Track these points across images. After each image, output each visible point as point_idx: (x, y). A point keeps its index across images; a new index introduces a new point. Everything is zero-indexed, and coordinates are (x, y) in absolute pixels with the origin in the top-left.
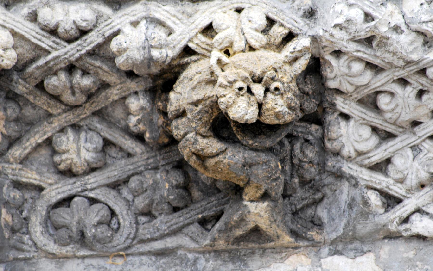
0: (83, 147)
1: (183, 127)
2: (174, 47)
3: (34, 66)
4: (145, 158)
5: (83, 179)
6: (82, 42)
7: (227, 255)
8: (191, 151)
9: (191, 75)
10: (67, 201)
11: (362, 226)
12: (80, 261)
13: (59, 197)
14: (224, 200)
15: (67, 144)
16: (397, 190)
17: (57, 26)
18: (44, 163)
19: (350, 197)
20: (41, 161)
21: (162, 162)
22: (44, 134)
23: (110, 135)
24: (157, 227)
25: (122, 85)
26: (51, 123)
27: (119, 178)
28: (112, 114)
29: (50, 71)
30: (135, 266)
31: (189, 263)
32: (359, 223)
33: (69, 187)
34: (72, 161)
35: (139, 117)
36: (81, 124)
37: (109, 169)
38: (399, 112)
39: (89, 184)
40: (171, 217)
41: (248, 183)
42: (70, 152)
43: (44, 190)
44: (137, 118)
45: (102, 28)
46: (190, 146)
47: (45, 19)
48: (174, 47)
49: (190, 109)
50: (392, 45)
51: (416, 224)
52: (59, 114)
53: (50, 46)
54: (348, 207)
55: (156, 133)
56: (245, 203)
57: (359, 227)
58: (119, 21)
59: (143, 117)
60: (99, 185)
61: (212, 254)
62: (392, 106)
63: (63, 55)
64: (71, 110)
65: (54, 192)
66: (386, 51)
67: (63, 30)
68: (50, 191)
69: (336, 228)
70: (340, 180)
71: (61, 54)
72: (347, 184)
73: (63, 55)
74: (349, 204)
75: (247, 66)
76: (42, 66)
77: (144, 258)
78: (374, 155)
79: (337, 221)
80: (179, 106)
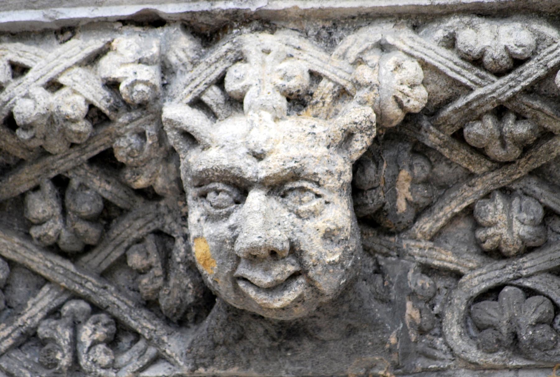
0: (516, 218)
3: (451, 108)
10: (493, 293)
17: (483, 53)
18: (463, 240)
20: (458, 237)
22: (464, 201)
26: (473, 185)
29: (472, 115)
33: (497, 273)
34: (501, 237)
37: (552, 249)
39: (524, 269)
42: (499, 225)
47: (467, 44)
52: (484, 174)
63: (490, 94)
64: (500, 168)
65: (476, 279)
71: (488, 92)
73: (490, 94)
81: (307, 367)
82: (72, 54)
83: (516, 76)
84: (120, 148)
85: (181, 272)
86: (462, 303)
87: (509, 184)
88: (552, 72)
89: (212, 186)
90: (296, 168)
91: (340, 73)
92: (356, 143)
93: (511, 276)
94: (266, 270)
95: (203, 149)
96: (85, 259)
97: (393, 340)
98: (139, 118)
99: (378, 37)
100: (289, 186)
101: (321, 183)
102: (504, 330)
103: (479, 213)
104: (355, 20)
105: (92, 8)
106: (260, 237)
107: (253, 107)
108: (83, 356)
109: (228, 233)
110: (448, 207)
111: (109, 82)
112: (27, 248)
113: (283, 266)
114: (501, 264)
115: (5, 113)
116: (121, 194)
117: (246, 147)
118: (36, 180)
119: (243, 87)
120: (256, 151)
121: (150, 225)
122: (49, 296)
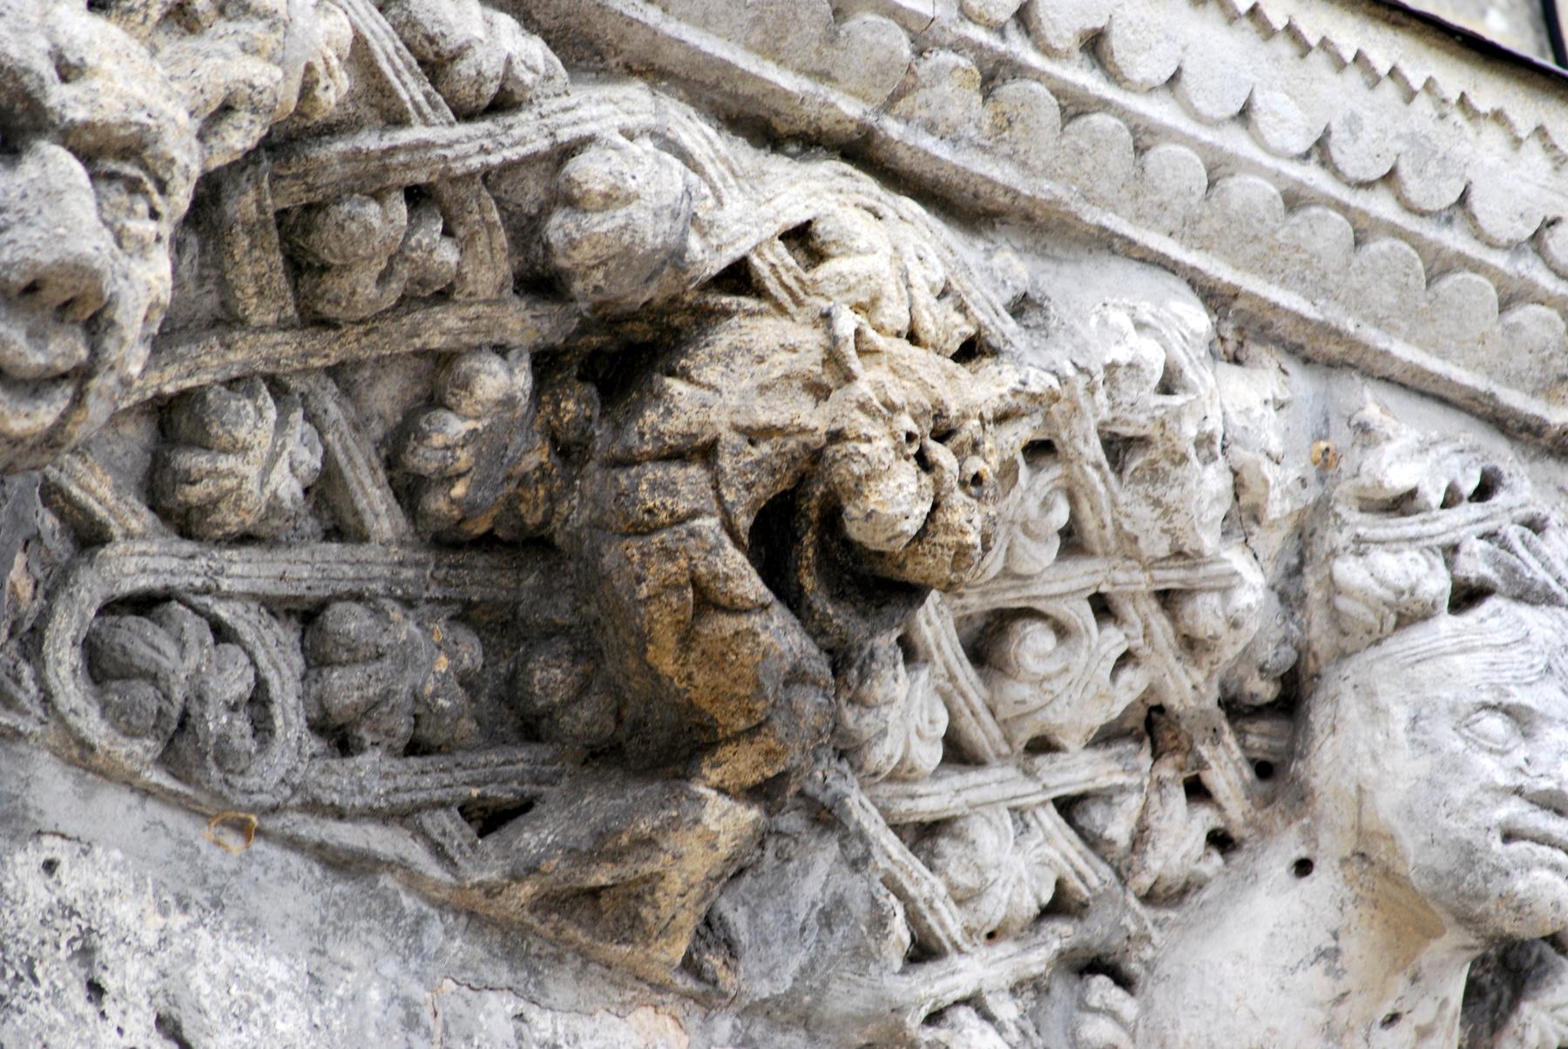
0: (291, 453)
1: (692, 492)
2: (719, 248)
3: (340, 146)
6: (499, 130)
7: (498, 938)
8: (693, 572)
9: (763, 345)
10: (146, 604)
11: (845, 989)
12: (133, 799)
13: (144, 583)
14: (547, 769)
15: (256, 427)
16: (949, 922)
17: (458, 54)
18: (119, 464)
19: (829, 891)
20: (112, 453)
21: (435, 591)
22: (190, 375)
23: (346, 450)
24: (360, 779)
25: (488, 310)
27: (306, 592)
29: (372, 181)
30: (271, 875)
31: (403, 923)
32: (841, 978)
33: (175, 563)
34: (241, 484)
36: (294, 384)
38: (1058, 691)
39: (228, 577)
40: (399, 765)
41: (752, 732)
42: (251, 454)
44: (471, 425)
46: (696, 555)
47: (440, 17)
48: (719, 248)
49: (734, 447)
50: (1183, 485)
51: (970, 1035)
52: (262, 329)
53: (416, 105)
54: (818, 920)
55: (487, 494)
56: (701, 789)
57: (837, 987)
58: (595, 112)
59: (489, 429)
61: (463, 920)
62: (1052, 667)
63: (442, 146)
65: (135, 560)
66: (1148, 496)
67: (473, 73)
69: (772, 969)
70: (821, 835)
71: (440, 141)
72: (833, 849)
73: (442, 146)
74: (822, 911)
75: (930, 381)
77: (295, 861)
78: (928, 795)
79: (777, 949)
80: (702, 425)
83: (499, 130)
86: (92, 602)
87: (285, 375)
90: (149, 128)
92: (232, 132)
93: (198, 582)
94: (36, 336)
100: (112, 165)
101: (170, 188)
102: (178, 695)
103: (218, 413)
106: (97, 249)
110: (156, 374)
113: (70, 339)
114: (187, 547)
117: (49, 38)
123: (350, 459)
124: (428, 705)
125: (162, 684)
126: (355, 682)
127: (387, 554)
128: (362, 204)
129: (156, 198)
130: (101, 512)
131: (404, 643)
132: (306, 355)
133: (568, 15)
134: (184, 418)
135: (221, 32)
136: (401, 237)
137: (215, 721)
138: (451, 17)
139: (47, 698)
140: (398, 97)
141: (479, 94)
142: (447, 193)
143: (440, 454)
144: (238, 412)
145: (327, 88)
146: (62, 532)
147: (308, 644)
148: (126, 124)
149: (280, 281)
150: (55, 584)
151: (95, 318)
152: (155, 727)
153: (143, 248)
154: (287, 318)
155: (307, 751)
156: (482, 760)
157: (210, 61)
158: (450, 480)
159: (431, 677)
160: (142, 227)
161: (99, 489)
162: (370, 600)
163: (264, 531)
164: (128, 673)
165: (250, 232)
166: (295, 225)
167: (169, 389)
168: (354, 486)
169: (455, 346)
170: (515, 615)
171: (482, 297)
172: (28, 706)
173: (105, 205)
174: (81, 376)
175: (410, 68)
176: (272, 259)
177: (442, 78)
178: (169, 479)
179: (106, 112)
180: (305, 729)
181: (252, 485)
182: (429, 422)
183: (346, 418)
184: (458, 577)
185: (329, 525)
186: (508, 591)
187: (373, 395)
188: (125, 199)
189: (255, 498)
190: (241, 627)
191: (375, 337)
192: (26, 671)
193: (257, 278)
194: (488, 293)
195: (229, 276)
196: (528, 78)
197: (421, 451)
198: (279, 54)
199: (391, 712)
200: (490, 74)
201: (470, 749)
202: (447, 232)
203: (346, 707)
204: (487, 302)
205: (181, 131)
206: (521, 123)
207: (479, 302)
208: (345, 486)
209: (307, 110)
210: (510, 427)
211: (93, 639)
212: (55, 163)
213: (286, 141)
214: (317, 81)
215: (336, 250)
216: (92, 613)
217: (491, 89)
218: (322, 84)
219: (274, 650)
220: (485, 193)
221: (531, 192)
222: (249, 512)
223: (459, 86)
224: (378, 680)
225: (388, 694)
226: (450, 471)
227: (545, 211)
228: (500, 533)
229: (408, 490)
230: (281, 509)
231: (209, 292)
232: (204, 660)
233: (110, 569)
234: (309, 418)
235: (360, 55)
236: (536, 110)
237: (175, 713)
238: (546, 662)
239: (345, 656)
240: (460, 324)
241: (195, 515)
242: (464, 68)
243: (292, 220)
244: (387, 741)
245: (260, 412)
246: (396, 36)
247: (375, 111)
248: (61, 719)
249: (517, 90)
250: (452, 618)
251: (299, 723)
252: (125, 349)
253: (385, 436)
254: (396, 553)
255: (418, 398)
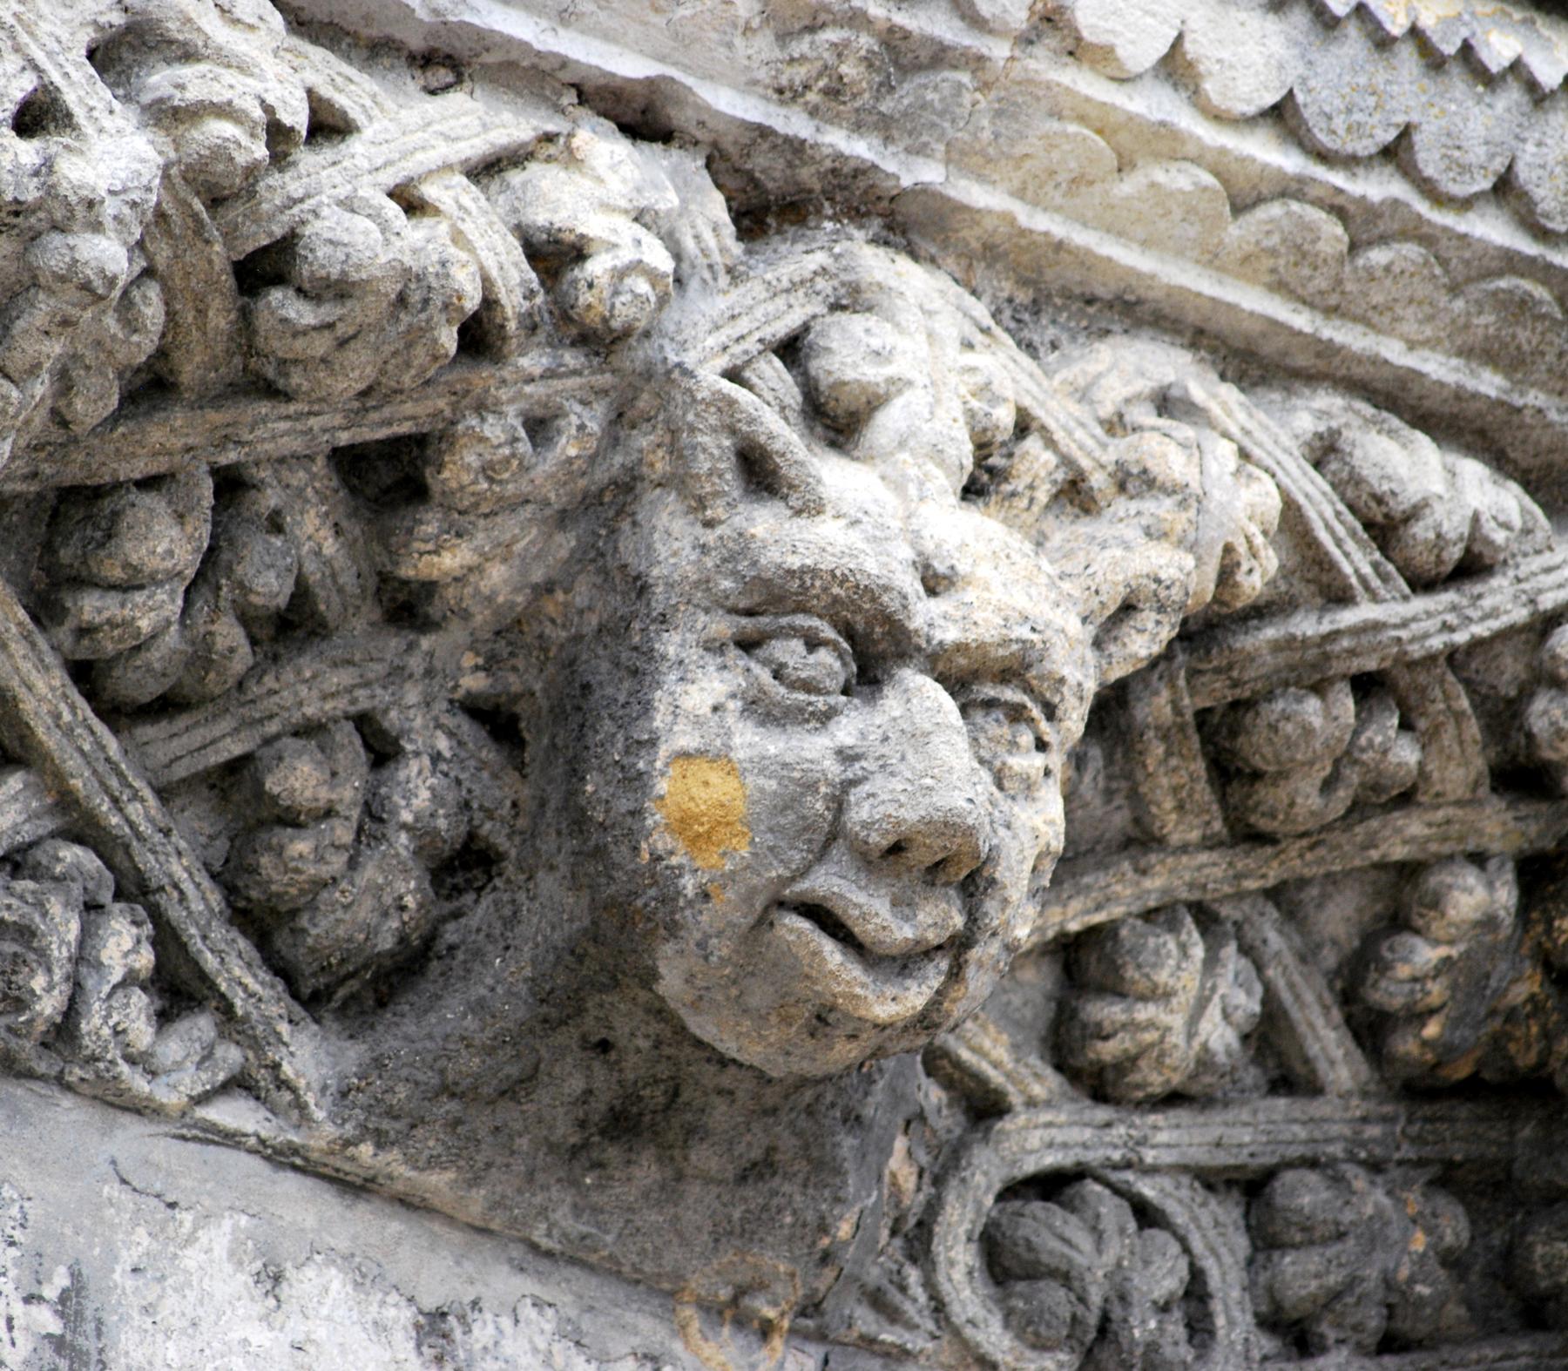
0: (1223, 997)
3: (1270, 632)
4: (1358, 1113)
5: (1138, 1121)
6: (1465, 602)
10: (1053, 1186)
13: (1051, 1160)
15: (1179, 967)
17: (1413, 514)
20: (1009, 1003)
21: (1407, 1151)
22: (1098, 908)
23: (1291, 986)
25: (1460, 813)
26: (1144, 872)
27: (1250, 1160)
28: (1311, 910)
29: (1311, 672)
33: (1088, 1134)
34: (1162, 1040)
35: (1454, 952)
36: (1225, 911)
37: (1230, 1115)
39: (1153, 1147)
42: (1174, 1001)
43: (1007, 1118)
44: (1443, 951)
45: (1534, 574)
47: (1389, 471)
52: (1184, 848)
53: (1363, 580)
59: (1467, 955)
60: (1183, 1161)
63: (1396, 626)
64: (1232, 846)
65: (1038, 1133)
67: (1431, 535)
68: (1026, 1128)
73: (1396, 626)
76: (1305, 642)
81: (607, 1232)
82: (460, 132)
83: (1465, 602)
84: (483, 440)
85: (397, 855)
86: (989, 1188)
88: (1546, 623)
89: (801, 620)
91: (1079, 434)
93: (1116, 1156)
95: (798, 513)
96: (146, 732)
97: (844, 1230)
98: (576, 373)
99: (1169, 376)
100: (989, 691)
101: (1059, 713)
102: (1095, 1298)
103: (1134, 952)
104: (1091, 310)
105: (544, 23)
106: (971, 801)
107: (912, 443)
108: (96, 1006)
109: (833, 768)
111: (557, 242)
112: (33, 645)
113: (944, 905)
114: (1102, 1113)
115: (278, 231)
116: (347, 579)
117: (913, 545)
118: (177, 458)
119: (891, 381)
120: (936, 564)
121: (361, 693)
122: (18, 806)
123: (1297, 997)
124: (1403, 1293)
125: (1076, 1284)
126: (1312, 1268)
127: (1347, 1109)
128: (1299, 700)
129: (1044, 726)
130: (996, 1078)
131: (1371, 1218)
132: (1239, 877)
133: (1551, 451)
134: (1093, 959)
135: (1121, 514)
136: (1348, 737)
137: (1142, 1327)
138: (1403, 471)
139: (939, 1307)
140: (1339, 571)
141: (1439, 561)
142: (1404, 679)
143: (1407, 987)
144: (1157, 952)
145: (1250, 571)
146: (950, 1105)
147: (1253, 1222)
148: (1006, 642)
149: (1204, 792)
150: (943, 1169)
151: (971, 876)
152: (1069, 1337)
153: (1028, 787)
154: (1214, 835)
155: (1256, 1354)
156: (1474, 1356)
157: (1107, 553)
158: (1419, 1016)
159: (1406, 1259)
160: (1028, 762)
161: (992, 1052)
162: (1327, 1165)
163: (1195, 1089)
164: (1034, 1272)
165: (1165, 737)
166: (1220, 725)
167: (1074, 927)
168: (1303, 1028)
169: (1420, 856)
170: (1509, 1177)
171: (1452, 798)
172: (917, 1319)
173: (983, 741)
174: (959, 945)
175: (1353, 534)
176: (1193, 767)
177: (1394, 543)
178: (1077, 1033)
179: (981, 630)
180: (1253, 1328)
181: (1177, 1038)
182: (1391, 949)
183: (1290, 948)
184: (1433, 1132)
185: (1275, 1073)
186: (1499, 1145)
187: (1323, 917)
188: (1005, 731)
189: (1181, 1052)
190: (1172, 1208)
191: (1322, 851)
192: (913, 1275)
193: (1175, 790)
194: (1460, 792)
195: (1143, 789)
196: (1500, 537)
197: (1383, 984)
198: (1191, 536)
199: (1358, 1303)
200: (1452, 535)
201: (1457, 1342)
202: (1406, 726)
203: (1302, 1299)
204: (1459, 803)
205: (1072, 643)
206: (1493, 591)
207: (1449, 804)
208: (1291, 1028)
209: (1227, 597)
210: (1492, 951)
211: (992, 1230)
212: (920, 697)
213: (1202, 632)
214: (1238, 564)
215: (1270, 756)
216: (989, 1200)
217: (1455, 553)
218: (1245, 567)
219: (1212, 1233)
220: (1450, 678)
221: (1509, 671)
222: (1175, 1069)
223: (1415, 553)
224: (1340, 1265)
225: (1352, 1282)
226: (1420, 1007)
227: (1526, 693)
228: (1487, 1075)
229: (1371, 1031)
230: (1213, 1064)
231: (1119, 808)
232: (1126, 1253)
233: (1010, 1146)
234: (1245, 950)
235: (1293, 521)
236: (1511, 573)
237: (1093, 1319)
238: (1548, 1234)
239: (1298, 1237)
240: (1427, 831)
241: (1110, 1075)
242: (1421, 531)
243: (1216, 719)
244: (1355, 1337)
245: (1183, 949)
246: (1335, 498)
247: (1312, 588)
248: (956, 1332)
249: (1487, 552)
250: (1431, 1183)
251: (1245, 1320)
252: (1009, 911)
253: (1340, 966)
254: (1358, 1108)
255: (1378, 918)
